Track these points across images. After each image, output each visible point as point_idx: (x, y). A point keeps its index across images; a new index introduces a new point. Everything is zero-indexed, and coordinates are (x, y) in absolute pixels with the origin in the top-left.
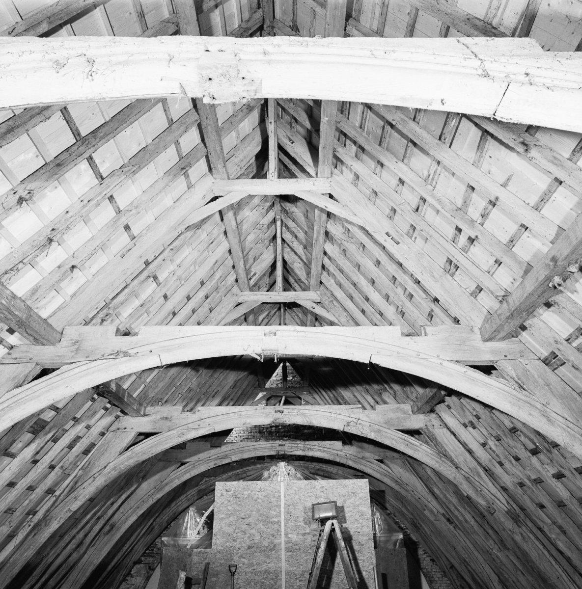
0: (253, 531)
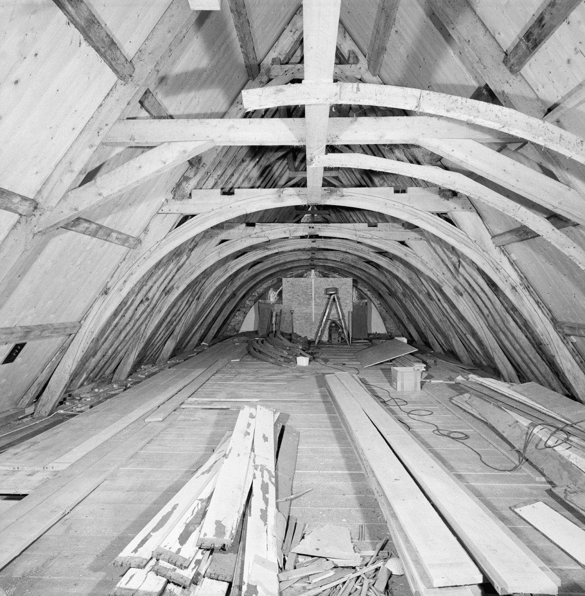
0: (300, 298)
